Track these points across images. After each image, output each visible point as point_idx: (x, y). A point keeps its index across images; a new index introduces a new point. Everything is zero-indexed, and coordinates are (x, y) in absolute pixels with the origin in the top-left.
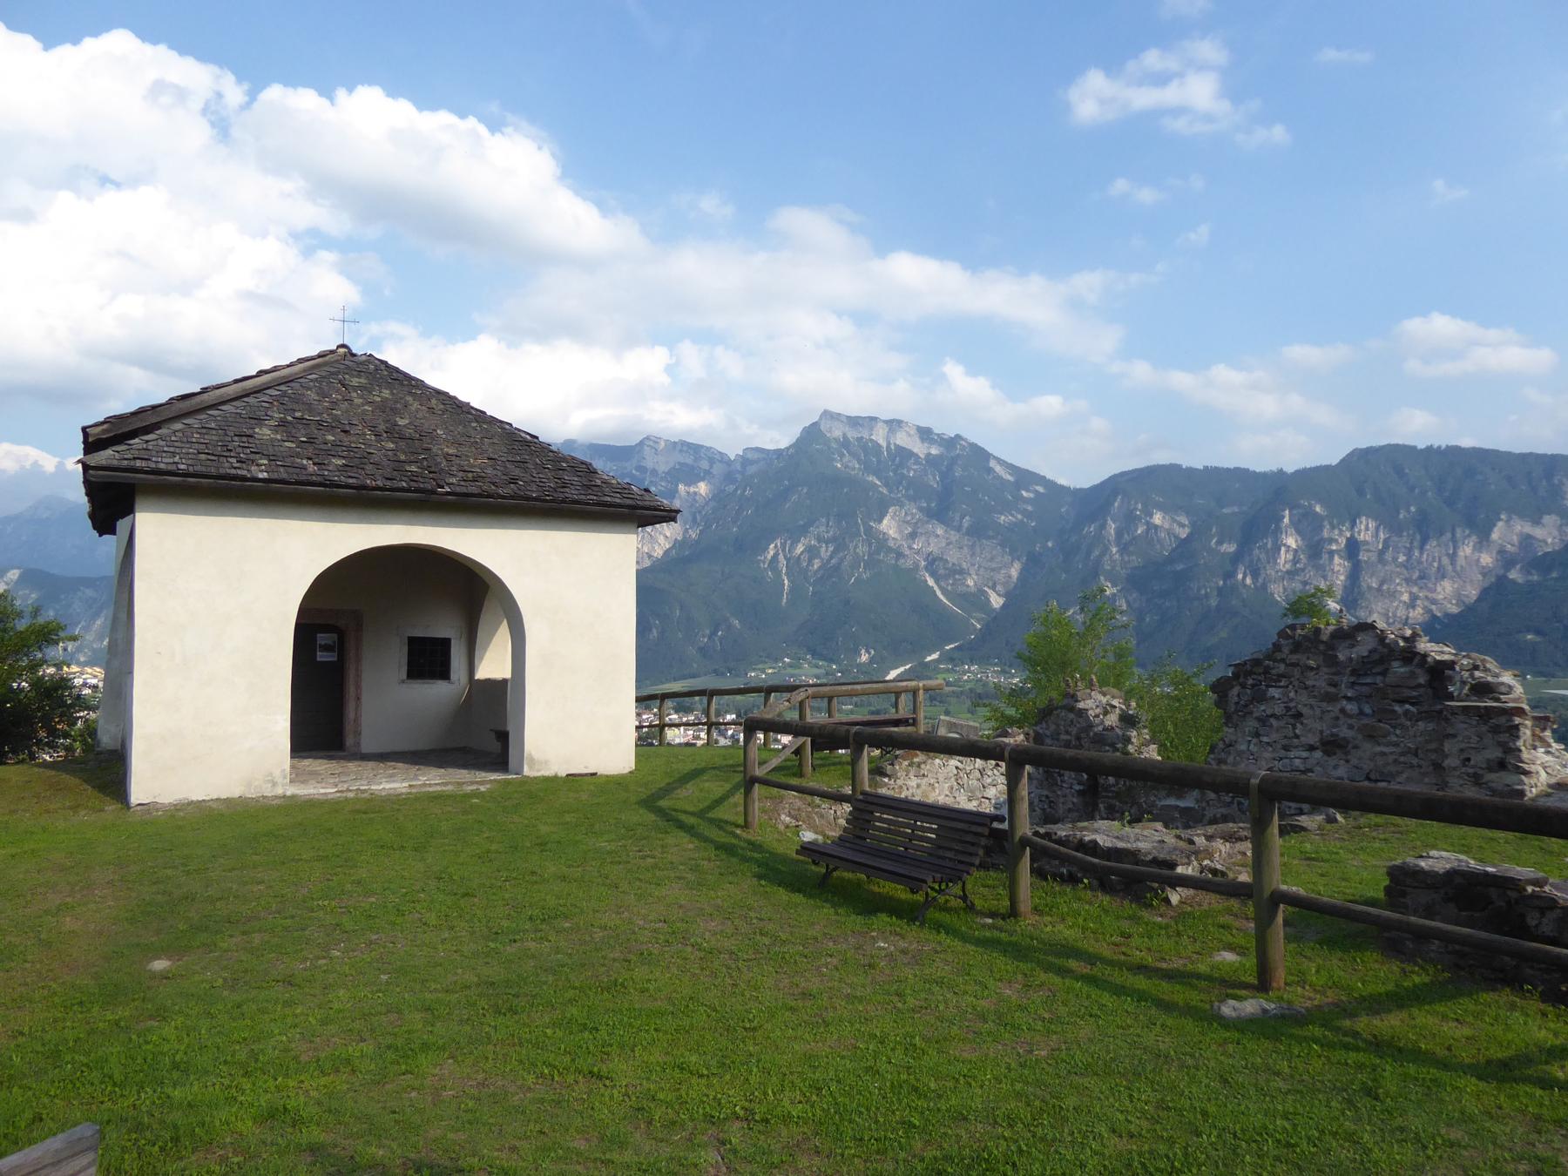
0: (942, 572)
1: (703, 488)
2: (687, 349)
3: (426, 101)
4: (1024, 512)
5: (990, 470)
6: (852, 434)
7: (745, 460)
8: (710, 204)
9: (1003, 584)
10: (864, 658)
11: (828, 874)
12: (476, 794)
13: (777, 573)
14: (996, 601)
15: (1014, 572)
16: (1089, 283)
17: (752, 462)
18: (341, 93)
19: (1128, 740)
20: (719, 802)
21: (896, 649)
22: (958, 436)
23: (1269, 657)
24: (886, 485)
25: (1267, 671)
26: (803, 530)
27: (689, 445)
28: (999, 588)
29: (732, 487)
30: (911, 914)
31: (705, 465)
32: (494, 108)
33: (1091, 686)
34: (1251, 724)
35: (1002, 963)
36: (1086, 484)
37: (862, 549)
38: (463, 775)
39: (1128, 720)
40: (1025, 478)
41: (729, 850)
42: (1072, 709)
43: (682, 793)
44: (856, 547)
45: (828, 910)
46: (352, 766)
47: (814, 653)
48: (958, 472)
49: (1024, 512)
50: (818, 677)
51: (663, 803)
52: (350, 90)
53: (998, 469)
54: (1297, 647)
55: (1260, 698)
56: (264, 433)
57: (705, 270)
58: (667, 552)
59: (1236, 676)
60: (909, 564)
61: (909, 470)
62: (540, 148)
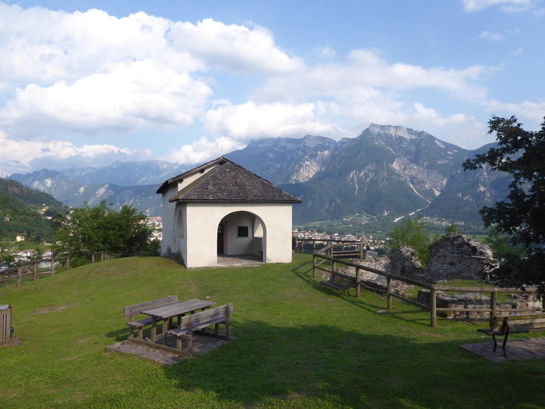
0: (416, 182)
1: (326, 152)
2: (320, 103)
3: (227, 22)
4: (449, 160)
5: (435, 144)
6: (382, 132)
7: (342, 143)
8: (327, 51)
9: (440, 187)
10: (386, 214)
11: (325, 287)
12: (256, 267)
13: (354, 183)
14: (437, 193)
15: (444, 182)
16: (474, 71)
17: (344, 143)
18: (199, 23)
19: (412, 259)
20: (309, 271)
21: (397, 211)
22: (423, 132)
23: (440, 242)
24: (395, 151)
25: (440, 245)
26: (363, 167)
27: (322, 137)
28: (438, 188)
29: (337, 152)
30: (338, 295)
31: (327, 144)
32: (250, 22)
33: (404, 245)
34: (436, 258)
35: (348, 303)
36: (474, 149)
37: (385, 174)
38: (252, 262)
39: (413, 254)
40: (449, 147)
41: (308, 282)
42: (399, 251)
43: (302, 268)
44: (383, 174)
45: (323, 294)
46: (227, 258)
47: (367, 212)
48: (422, 145)
49: (449, 160)
50: (368, 221)
51: (297, 271)
52: (202, 21)
53: (438, 143)
54: (446, 240)
55: (438, 251)
56: (210, 187)
57: (326, 75)
58: (314, 176)
59: (434, 246)
60: (403, 179)
61: (403, 144)
62: (267, 35)
